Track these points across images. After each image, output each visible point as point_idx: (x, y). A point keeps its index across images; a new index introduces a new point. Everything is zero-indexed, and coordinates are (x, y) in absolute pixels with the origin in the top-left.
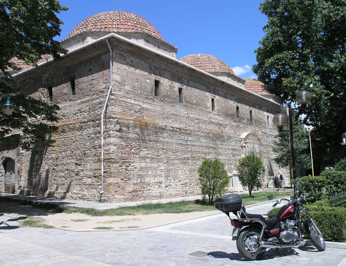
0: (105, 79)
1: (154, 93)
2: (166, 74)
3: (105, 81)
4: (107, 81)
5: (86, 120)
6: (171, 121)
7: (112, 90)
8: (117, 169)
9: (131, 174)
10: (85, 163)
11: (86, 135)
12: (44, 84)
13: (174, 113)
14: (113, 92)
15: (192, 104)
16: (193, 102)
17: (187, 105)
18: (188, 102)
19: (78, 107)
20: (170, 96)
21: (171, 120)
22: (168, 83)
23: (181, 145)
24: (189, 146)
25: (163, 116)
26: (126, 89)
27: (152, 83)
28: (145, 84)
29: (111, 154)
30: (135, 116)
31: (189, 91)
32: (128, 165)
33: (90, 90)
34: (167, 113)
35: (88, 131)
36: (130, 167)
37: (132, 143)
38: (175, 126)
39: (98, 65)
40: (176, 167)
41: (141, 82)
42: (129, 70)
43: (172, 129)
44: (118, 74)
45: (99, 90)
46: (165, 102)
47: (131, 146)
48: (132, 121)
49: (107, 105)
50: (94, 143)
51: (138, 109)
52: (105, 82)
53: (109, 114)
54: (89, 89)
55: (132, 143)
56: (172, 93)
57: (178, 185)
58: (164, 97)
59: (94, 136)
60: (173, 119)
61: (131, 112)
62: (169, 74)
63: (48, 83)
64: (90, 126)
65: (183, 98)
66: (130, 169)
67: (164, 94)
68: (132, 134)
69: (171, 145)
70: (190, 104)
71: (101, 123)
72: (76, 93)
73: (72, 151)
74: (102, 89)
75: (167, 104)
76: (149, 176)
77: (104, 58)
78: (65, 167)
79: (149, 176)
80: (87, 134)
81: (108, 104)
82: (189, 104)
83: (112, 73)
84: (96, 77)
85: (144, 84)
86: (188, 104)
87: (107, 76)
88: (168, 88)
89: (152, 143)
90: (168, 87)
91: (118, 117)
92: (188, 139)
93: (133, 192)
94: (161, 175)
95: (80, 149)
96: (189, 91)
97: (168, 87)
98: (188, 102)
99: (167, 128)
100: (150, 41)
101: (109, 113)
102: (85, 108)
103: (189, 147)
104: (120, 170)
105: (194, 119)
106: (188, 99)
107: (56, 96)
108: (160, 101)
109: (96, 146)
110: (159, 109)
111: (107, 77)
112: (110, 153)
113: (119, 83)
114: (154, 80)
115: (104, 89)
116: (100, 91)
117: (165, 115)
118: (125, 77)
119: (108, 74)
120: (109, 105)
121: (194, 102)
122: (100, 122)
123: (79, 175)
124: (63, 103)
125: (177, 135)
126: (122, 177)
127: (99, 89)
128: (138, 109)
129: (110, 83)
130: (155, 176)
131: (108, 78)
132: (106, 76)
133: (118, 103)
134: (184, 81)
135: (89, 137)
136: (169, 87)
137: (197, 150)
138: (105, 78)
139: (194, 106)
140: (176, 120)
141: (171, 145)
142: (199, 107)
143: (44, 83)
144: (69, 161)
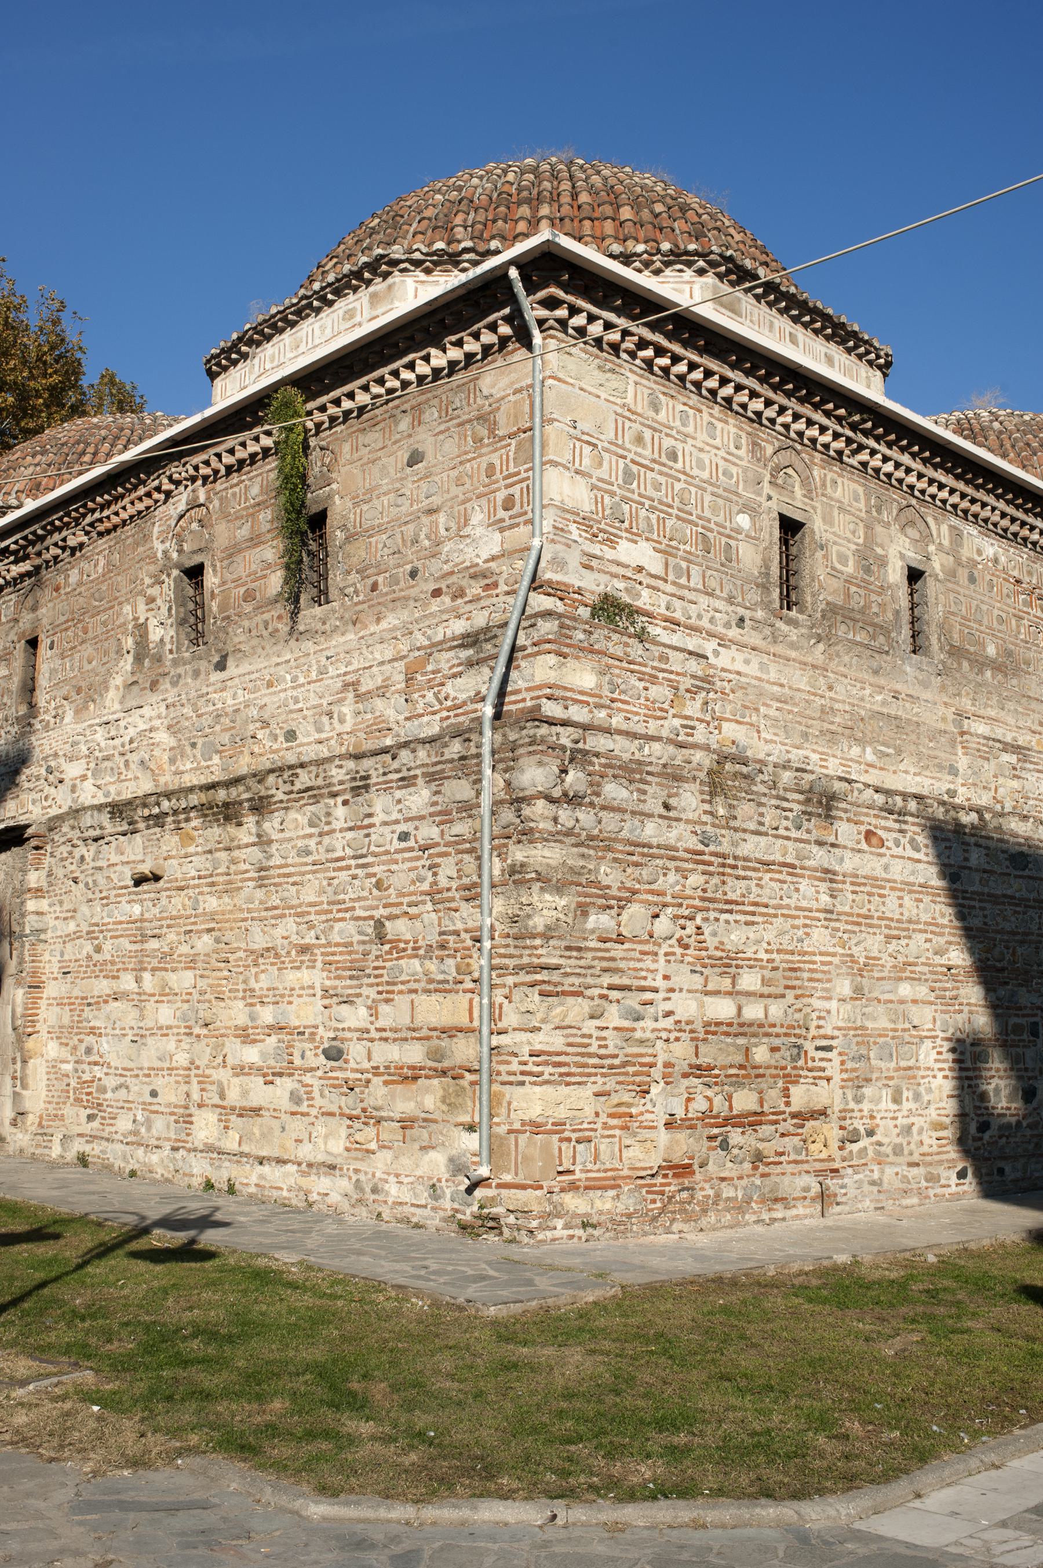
0: (499, 503)
1: (776, 594)
2: (840, 489)
3: (501, 514)
4: (510, 513)
5: (389, 742)
6: (870, 756)
7: (543, 564)
8: (574, 1031)
9: (652, 1065)
10: (380, 993)
11: (387, 830)
12: (160, 555)
13: (885, 711)
14: (548, 575)
15: (980, 663)
16: (984, 650)
17: (955, 666)
18: (956, 652)
19: (343, 670)
20: (862, 611)
21: (869, 750)
22: (849, 541)
23: (928, 894)
24: (972, 903)
25: (826, 726)
26: (623, 559)
27: (765, 535)
28: (729, 537)
29: (538, 942)
30: (674, 716)
31: (962, 590)
32: (638, 1007)
33: (413, 574)
34: (847, 708)
35: (399, 801)
36: (648, 1024)
37: (662, 878)
38: (892, 782)
39: (330, 785)
40: (907, 1026)
41: (703, 527)
42: (639, 450)
43: (880, 799)
44: (577, 472)
45: (467, 568)
46: (836, 644)
47: (652, 892)
48: (656, 746)
49: (514, 649)
50: (435, 874)
51: (693, 677)
52: (502, 520)
53: (524, 700)
54: (408, 567)
55: (662, 878)
56: (874, 597)
57: (915, 1129)
58: (829, 615)
59: (434, 832)
60: (884, 744)
61: (654, 691)
62: (856, 486)
63: (180, 551)
64: (415, 777)
65: (933, 628)
66: (648, 1035)
67: (829, 598)
68: (660, 821)
69: (874, 890)
70: (969, 660)
71: (479, 755)
72: (333, 593)
73: (307, 918)
74: (487, 561)
75: (846, 659)
76: (758, 1076)
77: (493, 387)
78: (267, 1015)
79: (758, 1076)
80: (397, 822)
81: (520, 642)
82: (965, 664)
83: (543, 464)
84: (447, 496)
85: (724, 540)
86: (960, 664)
87: (512, 485)
88: (850, 569)
89: (771, 879)
90: (851, 563)
91: (576, 718)
92: (966, 859)
93: (665, 1176)
94: (823, 1070)
95: (353, 909)
96: (962, 590)
97: (851, 563)
98: (959, 649)
99: (856, 793)
100: (744, 304)
101: (524, 695)
102: (382, 673)
103: (974, 907)
104: (590, 1036)
105: (998, 745)
106: (956, 636)
107: (223, 619)
108: (810, 637)
109: (449, 889)
110: (801, 680)
111: (511, 491)
112: (533, 937)
113: (585, 522)
114: (776, 515)
115: (493, 558)
116: (472, 571)
117: (837, 720)
118: (615, 488)
119: (518, 473)
120: (524, 648)
121: (991, 650)
122: (473, 751)
123: (346, 1062)
124: (260, 650)
125: (910, 834)
126: (600, 1080)
127: (467, 564)
128: (693, 677)
129: (531, 522)
130: (789, 1075)
131: (517, 496)
132: (507, 487)
133: (581, 636)
134: (935, 533)
135: (404, 837)
136: (857, 563)
137: (1008, 927)
138: (501, 496)
139: (988, 674)
140: (899, 752)
141: (874, 890)
142: (1014, 682)
143: (159, 547)
144: (292, 977)
